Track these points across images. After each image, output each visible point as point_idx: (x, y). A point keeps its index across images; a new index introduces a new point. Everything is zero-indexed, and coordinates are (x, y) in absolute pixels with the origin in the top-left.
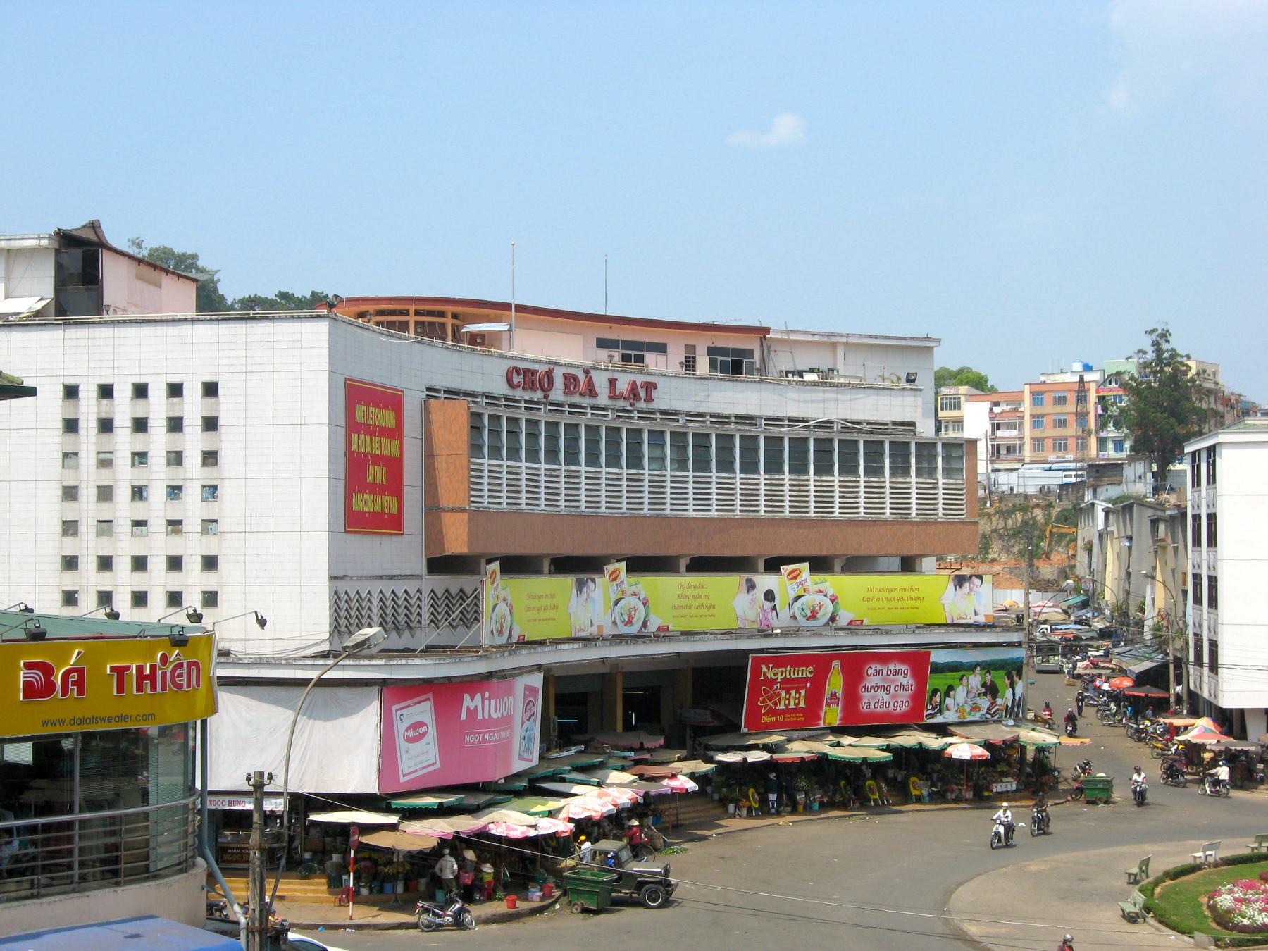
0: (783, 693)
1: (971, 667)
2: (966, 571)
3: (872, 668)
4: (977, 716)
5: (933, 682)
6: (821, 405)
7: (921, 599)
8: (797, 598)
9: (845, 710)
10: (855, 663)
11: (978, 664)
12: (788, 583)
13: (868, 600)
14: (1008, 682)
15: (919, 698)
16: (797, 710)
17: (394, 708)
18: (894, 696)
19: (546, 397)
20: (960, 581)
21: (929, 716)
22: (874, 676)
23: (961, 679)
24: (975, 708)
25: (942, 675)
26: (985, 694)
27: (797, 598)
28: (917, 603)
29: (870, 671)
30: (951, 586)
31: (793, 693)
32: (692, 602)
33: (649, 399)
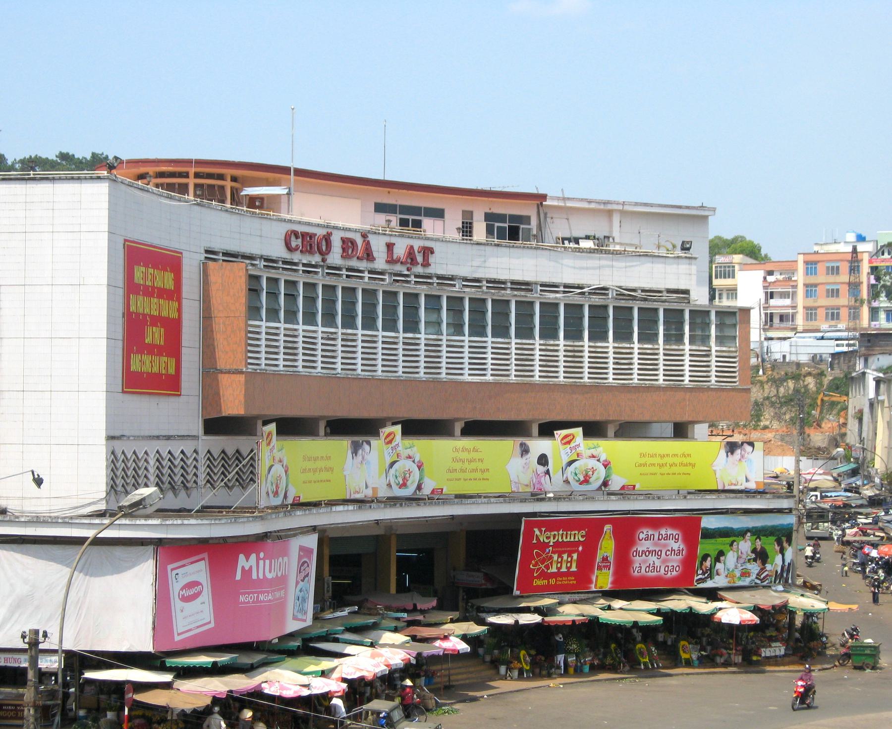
0: (555, 557)
1: (742, 533)
2: (737, 438)
3: (644, 532)
4: (746, 582)
5: (704, 547)
7: (693, 465)
8: (570, 463)
9: (616, 573)
10: (627, 528)
11: (748, 530)
12: (562, 447)
13: (640, 465)
14: (778, 548)
15: (689, 563)
16: (568, 574)
17: (170, 567)
18: (664, 561)
19: (324, 260)
20: (732, 448)
23: (731, 545)
24: (745, 574)
25: (713, 541)
26: (755, 560)
27: (570, 463)
29: (642, 536)
30: (723, 453)
33: (426, 264)
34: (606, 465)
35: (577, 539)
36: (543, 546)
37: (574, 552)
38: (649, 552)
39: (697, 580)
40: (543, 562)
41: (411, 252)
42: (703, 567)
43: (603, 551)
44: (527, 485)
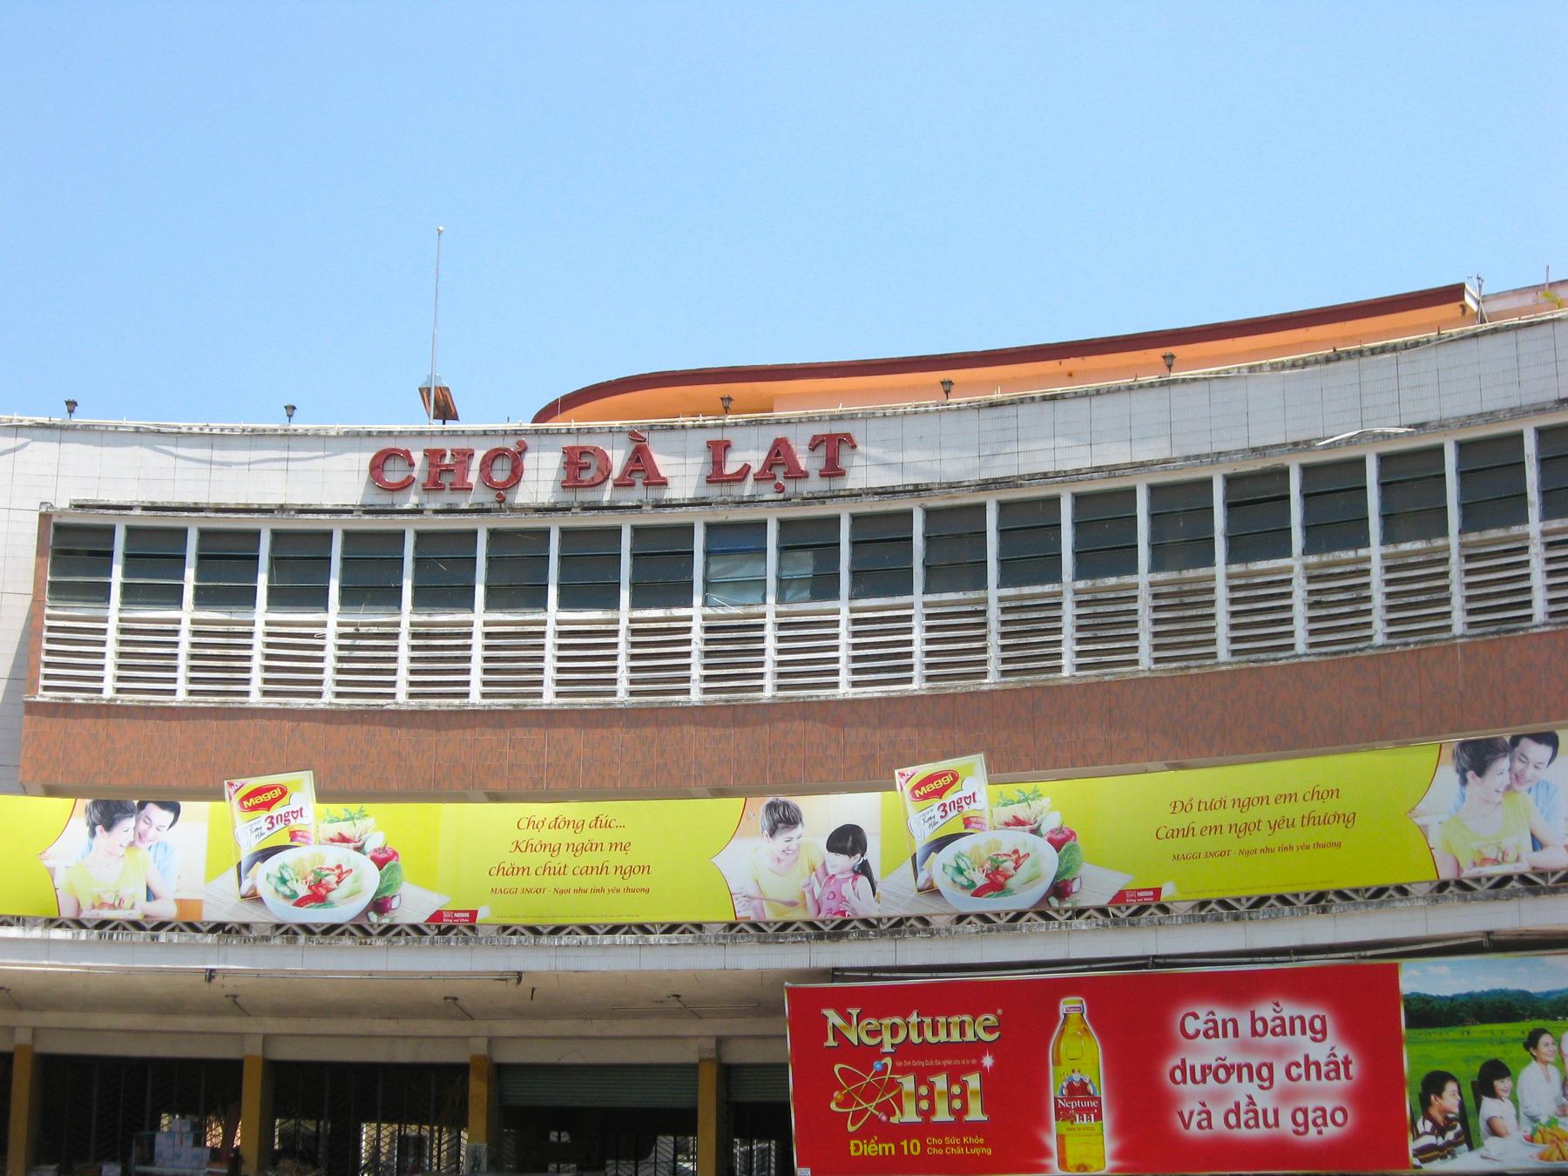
0: (908, 1083)
3: (1197, 1017)
5: (1418, 1054)
6: (298, 425)
7: (1348, 820)
8: (940, 844)
9: (1123, 1127)
10: (1136, 1009)
12: (912, 807)
13: (1174, 833)
16: (959, 1126)
18: (1286, 1096)
19: (501, 500)
20: (1477, 758)
21: (1426, 1153)
22: (1204, 1040)
23: (1532, 1042)
25: (1454, 1033)
27: (940, 844)
28: (1334, 832)
29: (1191, 1025)
31: (941, 1082)
32: (565, 857)
33: (833, 470)
34: (1060, 841)
35: (970, 1037)
36: (865, 1055)
37: (970, 1070)
38: (1229, 1070)
39: (1419, 1152)
40: (869, 1094)
41: (780, 454)
42: (1434, 1112)
43: (1066, 1068)
44: (793, 904)
